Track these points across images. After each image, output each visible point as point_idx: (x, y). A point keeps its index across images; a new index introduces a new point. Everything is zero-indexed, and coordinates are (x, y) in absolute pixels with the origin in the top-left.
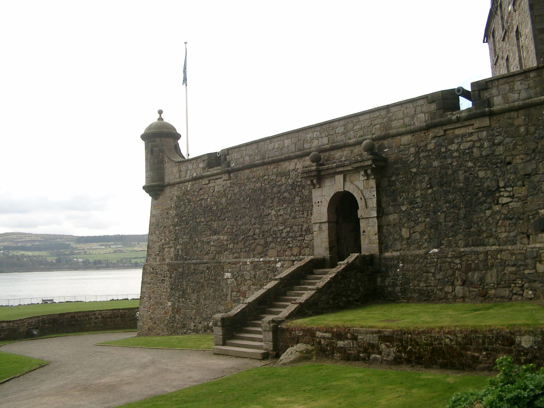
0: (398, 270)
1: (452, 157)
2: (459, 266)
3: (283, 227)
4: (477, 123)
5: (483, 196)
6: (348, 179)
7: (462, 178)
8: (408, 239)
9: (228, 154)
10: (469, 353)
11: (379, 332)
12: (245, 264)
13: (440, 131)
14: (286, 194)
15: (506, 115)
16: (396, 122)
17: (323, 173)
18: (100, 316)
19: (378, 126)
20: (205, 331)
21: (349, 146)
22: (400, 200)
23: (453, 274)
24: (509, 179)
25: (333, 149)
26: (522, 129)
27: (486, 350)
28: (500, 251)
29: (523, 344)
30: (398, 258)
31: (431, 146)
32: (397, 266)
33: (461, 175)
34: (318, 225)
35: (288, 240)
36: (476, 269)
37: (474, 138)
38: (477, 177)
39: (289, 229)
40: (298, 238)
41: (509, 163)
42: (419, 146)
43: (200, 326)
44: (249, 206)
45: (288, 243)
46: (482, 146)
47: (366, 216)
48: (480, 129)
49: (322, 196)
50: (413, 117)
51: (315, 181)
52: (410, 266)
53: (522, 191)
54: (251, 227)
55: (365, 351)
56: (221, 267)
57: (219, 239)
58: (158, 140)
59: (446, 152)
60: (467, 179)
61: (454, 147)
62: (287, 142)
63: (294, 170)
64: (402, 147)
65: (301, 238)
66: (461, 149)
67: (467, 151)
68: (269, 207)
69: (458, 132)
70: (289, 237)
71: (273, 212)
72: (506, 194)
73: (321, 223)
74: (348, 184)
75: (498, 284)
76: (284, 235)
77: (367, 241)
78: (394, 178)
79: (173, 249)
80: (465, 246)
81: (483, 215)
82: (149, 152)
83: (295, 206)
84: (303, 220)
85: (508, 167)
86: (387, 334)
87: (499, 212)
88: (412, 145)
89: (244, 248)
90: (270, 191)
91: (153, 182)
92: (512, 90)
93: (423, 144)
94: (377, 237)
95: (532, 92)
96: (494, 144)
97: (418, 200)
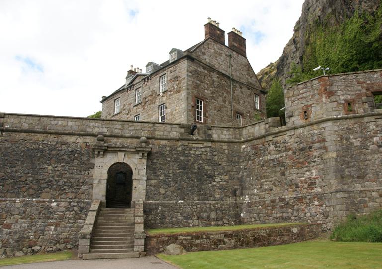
1: (191, 157)
2: (196, 210)
3: (60, 179)
4: (205, 144)
5: (207, 177)
6: (126, 155)
7: (196, 167)
8: (163, 194)
9: (4, 118)
10: (272, 238)
11: (225, 233)
12: (15, 202)
13: (186, 143)
14: (65, 157)
15: (219, 143)
17: (109, 149)
21: (125, 137)
22: (159, 173)
23: (193, 214)
24: (220, 172)
25: (111, 136)
26: (226, 151)
27: (279, 235)
28: (218, 203)
29: (294, 231)
31: (179, 149)
32: (157, 209)
33: (196, 166)
34: (98, 180)
35: (64, 187)
36: (206, 211)
37: (203, 150)
38: (204, 168)
40: (75, 187)
41: (220, 165)
45: (64, 190)
46: (207, 155)
48: (206, 147)
49: (102, 167)
50: (169, 132)
51: (102, 153)
53: (227, 177)
54: (22, 174)
55: (215, 243)
59: (188, 153)
60: (199, 168)
61: (192, 152)
62: (70, 123)
63: (74, 142)
65: (78, 188)
68: (46, 163)
69: (194, 145)
70: (66, 186)
71: (50, 167)
72: (219, 178)
73: (101, 179)
75: (217, 219)
76: (61, 184)
77: (137, 193)
78: (155, 161)
80: (198, 200)
81: (207, 186)
85: (220, 166)
86: (229, 233)
87: (215, 185)
89: (12, 190)
90: (48, 152)
92: (222, 133)
93: (175, 147)
95: (231, 137)
96: (213, 155)
97: (171, 175)
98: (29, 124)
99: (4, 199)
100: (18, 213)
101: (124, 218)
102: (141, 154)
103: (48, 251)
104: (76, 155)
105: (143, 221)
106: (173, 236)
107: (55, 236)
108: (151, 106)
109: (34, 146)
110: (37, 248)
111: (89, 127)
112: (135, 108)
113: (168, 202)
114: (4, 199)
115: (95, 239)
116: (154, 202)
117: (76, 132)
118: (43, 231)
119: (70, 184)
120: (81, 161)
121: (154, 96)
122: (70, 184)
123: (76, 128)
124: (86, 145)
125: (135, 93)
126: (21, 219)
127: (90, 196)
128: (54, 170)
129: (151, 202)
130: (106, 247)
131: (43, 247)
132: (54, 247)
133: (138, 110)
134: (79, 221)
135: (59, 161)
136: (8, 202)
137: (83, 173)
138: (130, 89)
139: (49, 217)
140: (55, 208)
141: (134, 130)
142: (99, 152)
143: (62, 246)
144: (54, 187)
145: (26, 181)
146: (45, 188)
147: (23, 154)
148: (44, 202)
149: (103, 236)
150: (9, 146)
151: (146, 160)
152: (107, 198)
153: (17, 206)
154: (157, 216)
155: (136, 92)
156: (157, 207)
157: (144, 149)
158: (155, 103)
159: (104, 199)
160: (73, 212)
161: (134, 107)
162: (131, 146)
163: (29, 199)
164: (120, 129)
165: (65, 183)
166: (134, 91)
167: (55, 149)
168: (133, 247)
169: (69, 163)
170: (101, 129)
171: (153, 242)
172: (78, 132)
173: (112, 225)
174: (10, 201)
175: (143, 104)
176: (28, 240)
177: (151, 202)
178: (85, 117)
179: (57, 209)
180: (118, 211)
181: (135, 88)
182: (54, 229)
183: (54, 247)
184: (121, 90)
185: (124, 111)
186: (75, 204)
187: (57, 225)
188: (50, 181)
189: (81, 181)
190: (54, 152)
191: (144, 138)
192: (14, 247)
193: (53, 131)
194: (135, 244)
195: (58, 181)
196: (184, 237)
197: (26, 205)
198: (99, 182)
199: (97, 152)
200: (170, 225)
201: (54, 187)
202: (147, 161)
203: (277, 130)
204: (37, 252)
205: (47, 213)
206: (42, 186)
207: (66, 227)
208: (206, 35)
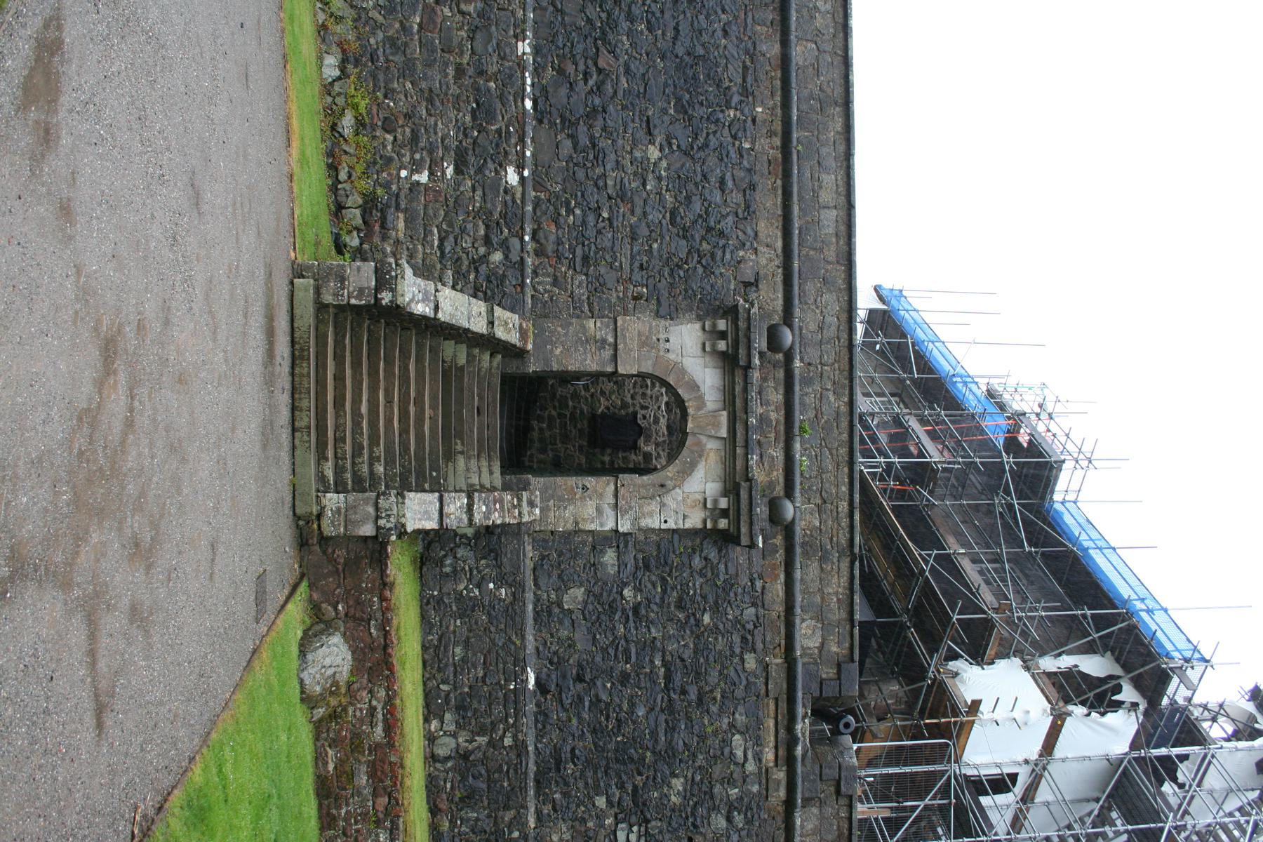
0: (491, 586)
14: (697, 207)
32: (501, 580)
42: (756, 632)
51: (722, 345)
64: (759, 584)
66: (733, 735)
67: (727, 751)
88: (761, 611)
102: (723, 503)
134: (450, 273)
141: (821, 471)
142: (723, 335)
144: (581, 174)
148: (522, 140)
149: (389, 362)
151: (699, 526)
154: (470, 580)
157: (744, 518)
159: (533, 367)
182: (418, 183)
188: (600, 157)
199: (722, 325)
206: (582, 128)
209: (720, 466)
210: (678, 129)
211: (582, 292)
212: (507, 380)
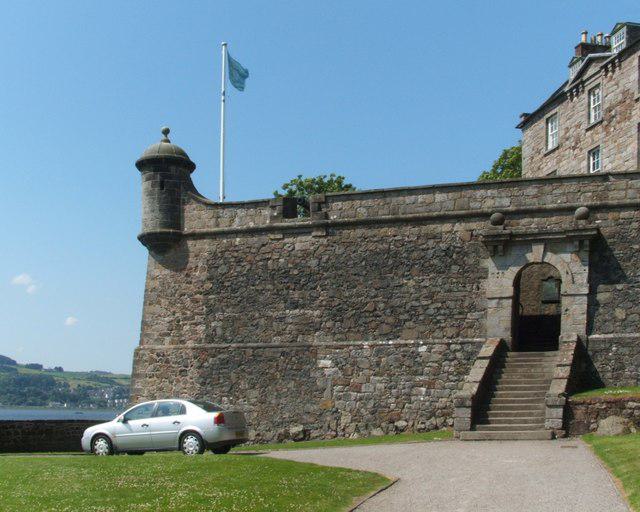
12: (361, 347)
14: (436, 261)
16: (615, 192)
18: (19, 431)
19: (590, 194)
20: (280, 441)
30: (611, 341)
32: (608, 350)
35: (438, 318)
39: (440, 305)
43: (269, 435)
44: (364, 272)
45: (439, 321)
47: (573, 293)
51: (500, 247)
52: (626, 350)
54: (368, 300)
56: (312, 352)
57: (304, 314)
58: (173, 169)
62: (439, 197)
64: (621, 221)
65: (461, 316)
68: (403, 276)
71: (412, 283)
73: (501, 298)
74: (549, 254)
76: (431, 311)
79: (202, 328)
82: (158, 184)
83: (450, 277)
84: (464, 293)
89: (355, 327)
91: (163, 228)
94: (585, 316)
98: (368, 208)
99: (345, 343)
100: (368, 366)
101: (539, 370)
102: (577, 243)
103: (419, 430)
104: (454, 256)
105: (567, 375)
106: (615, 402)
107: (427, 403)
108: (623, 124)
109: (381, 246)
110: (401, 424)
111: (475, 200)
112: (589, 133)
113: (632, 335)
114: (345, 343)
115: (481, 410)
116: (602, 336)
117: (450, 213)
118: (409, 395)
119: (447, 312)
120: (458, 265)
121: (628, 102)
122: (447, 312)
123: (450, 205)
124: (472, 235)
125: (587, 99)
126: (375, 375)
127: (482, 330)
128: (418, 288)
129: (597, 336)
130: (500, 422)
131: (411, 423)
132: (428, 423)
133: (596, 137)
135: (424, 270)
136: (351, 348)
137: (468, 289)
138: (578, 91)
139: (416, 371)
140: (425, 355)
141: (564, 194)
143: (439, 421)
144: (421, 318)
145: (375, 310)
146: (406, 321)
147: (363, 263)
148: (406, 345)
150: (341, 251)
152: (514, 334)
153: (366, 353)
155: (589, 98)
156: (608, 345)
157: (584, 233)
158: (629, 118)
159: (508, 336)
160: (456, 362)
161: (587, 130)
162: (556, 229)
163: (382, 340)
164: (535, 196)
165: (439, 309)
166: (585, 96)
167: (416, 248)
168: (543, 421)
169: (444, 272)
170: (498, 200)
171: (579, 412)
172: (456, 213)
173: (516, 383)
174: (354, 346)
175: (605, 123)
176: (387, 410)
177: (597, 336)
178: (473, 178)
179: (428, 357)
180: (532, 356)
181: (587, 89)
182: (427, 392)
183: (428, 423)
184: (558, 97)
185: (568, 142)
186: (458, 347)
187: (430, 385)
188: (414, 308)
189: (466, 304)
190: (415, 254)
191: (581, 210)
192: (368, 420)
193: (410, 216)
194: (547, 416)
195: (426, 308)
196: (635, 404)
197: (380, 351)
198: (498, 303)
200: (633, 382)
201: (421, 318)
202: (590, 255)
203: (92, 384)
204: (402, 431)
205: (412, 363)
206: (402, 317)
207: (444, 388)
208: (148, 302)
209: (157, 214)
210: (400, 272)
211: (476, 315)
212: (515, 349)
